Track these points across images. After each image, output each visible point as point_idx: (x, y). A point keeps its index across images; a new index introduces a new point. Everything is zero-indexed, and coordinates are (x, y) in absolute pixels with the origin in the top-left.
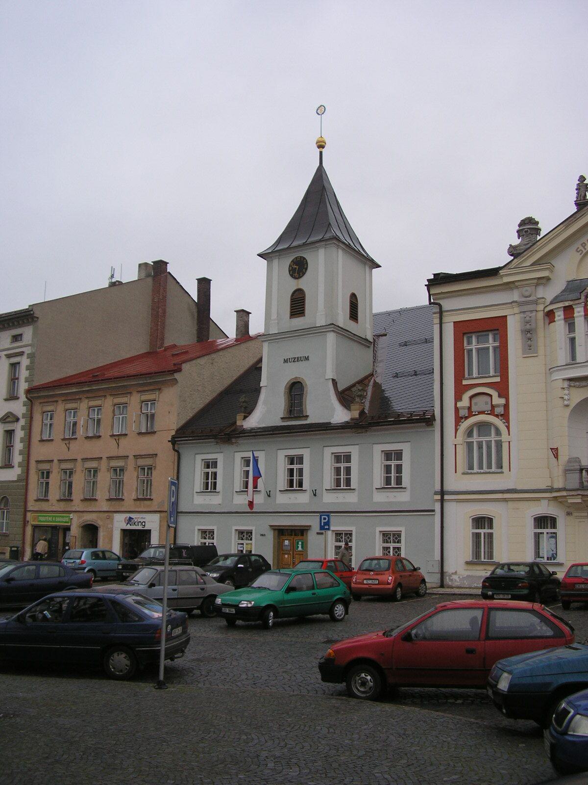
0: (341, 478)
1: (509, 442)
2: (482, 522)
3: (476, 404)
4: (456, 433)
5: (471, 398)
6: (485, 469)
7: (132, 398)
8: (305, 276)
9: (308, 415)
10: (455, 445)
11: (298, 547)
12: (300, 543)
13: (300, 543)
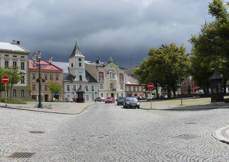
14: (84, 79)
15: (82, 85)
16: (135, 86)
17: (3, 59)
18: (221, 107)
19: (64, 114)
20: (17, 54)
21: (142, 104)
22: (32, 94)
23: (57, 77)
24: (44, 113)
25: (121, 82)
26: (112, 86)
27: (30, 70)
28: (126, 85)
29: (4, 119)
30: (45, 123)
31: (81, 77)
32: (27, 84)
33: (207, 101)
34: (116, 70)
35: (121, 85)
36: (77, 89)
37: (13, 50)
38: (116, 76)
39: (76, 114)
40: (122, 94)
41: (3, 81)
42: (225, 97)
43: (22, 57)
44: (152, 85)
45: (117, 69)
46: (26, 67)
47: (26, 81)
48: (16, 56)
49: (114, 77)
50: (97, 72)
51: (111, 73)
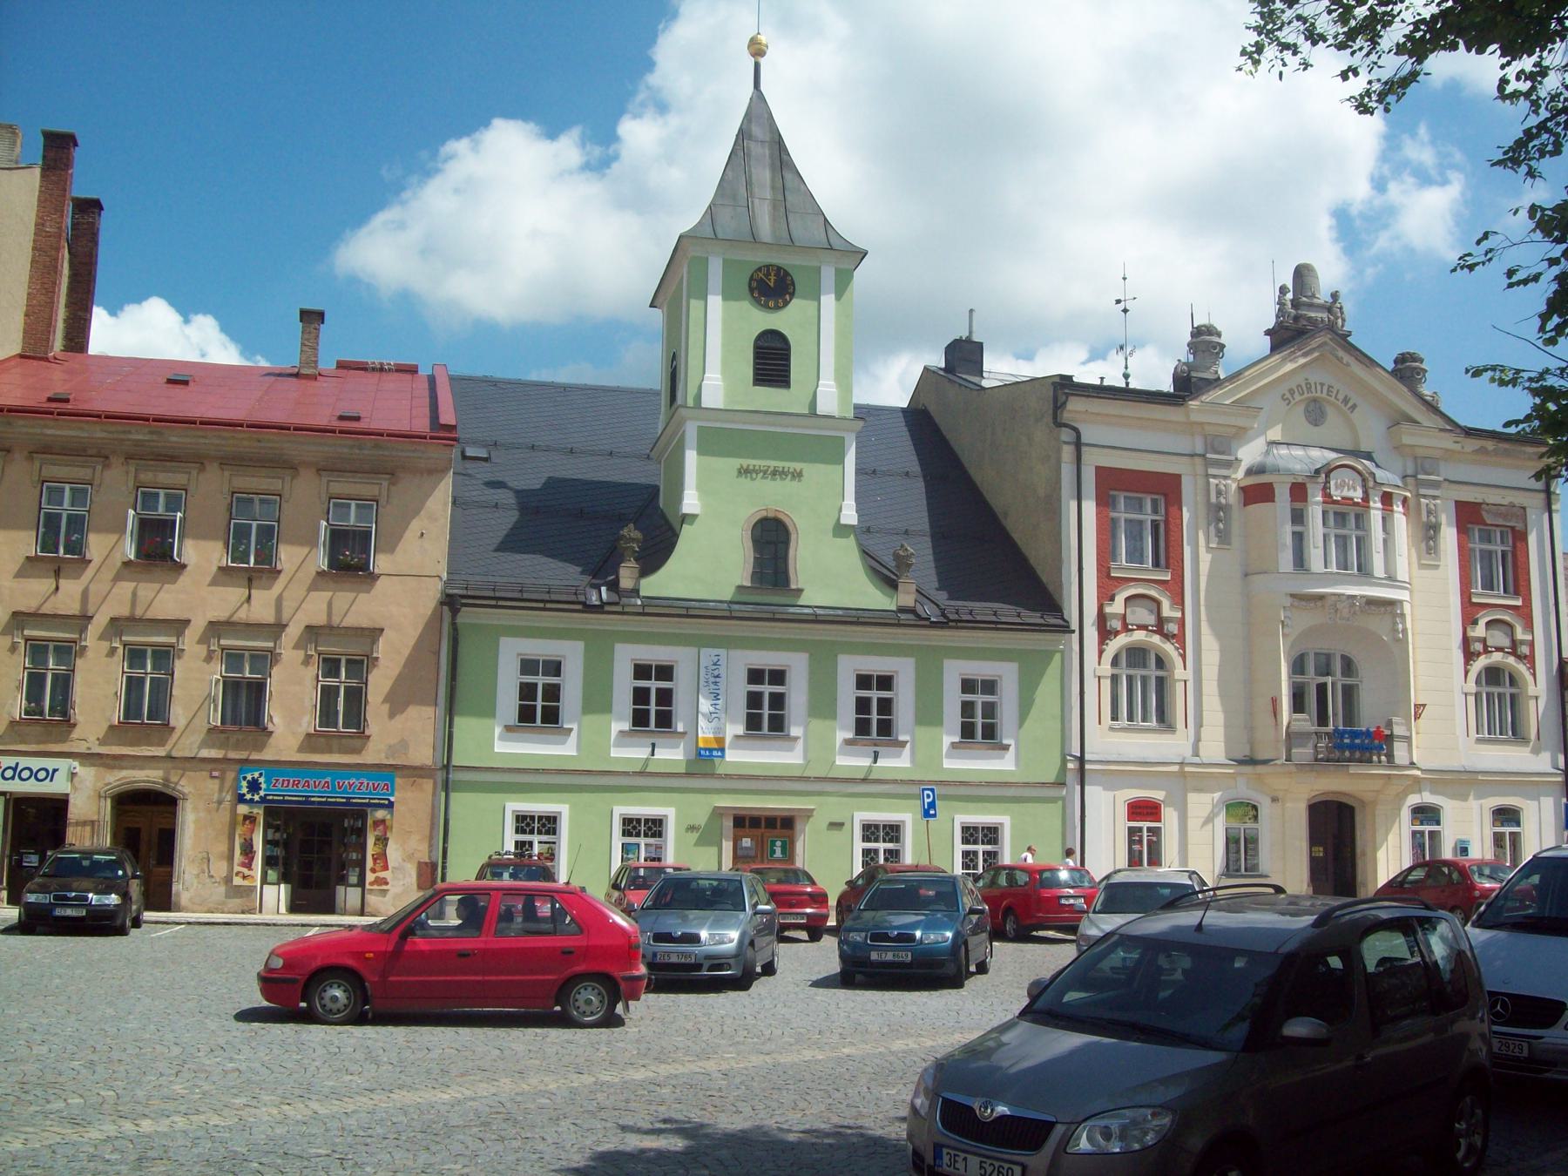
0: (535, 706)
1: (1185, 681)
2: (1143, 810)
3: (1133, 612)
4: (1100, 657)
5: (1127, 600)
6: (1123, 721)
7: (295, 481)
8: (747, 288)
9: (800, 587)
10: (1099, 677)
11: (774, 852)
12: (779, 843)
13: (779, 843)
18: (229, 702)
24: (1096, 1112)
25: (1479, 631)
35: (1136, 655)
40: (1506, 815)
45: (1408, 437)
50: (1067, 471)
51: (1299, 492)
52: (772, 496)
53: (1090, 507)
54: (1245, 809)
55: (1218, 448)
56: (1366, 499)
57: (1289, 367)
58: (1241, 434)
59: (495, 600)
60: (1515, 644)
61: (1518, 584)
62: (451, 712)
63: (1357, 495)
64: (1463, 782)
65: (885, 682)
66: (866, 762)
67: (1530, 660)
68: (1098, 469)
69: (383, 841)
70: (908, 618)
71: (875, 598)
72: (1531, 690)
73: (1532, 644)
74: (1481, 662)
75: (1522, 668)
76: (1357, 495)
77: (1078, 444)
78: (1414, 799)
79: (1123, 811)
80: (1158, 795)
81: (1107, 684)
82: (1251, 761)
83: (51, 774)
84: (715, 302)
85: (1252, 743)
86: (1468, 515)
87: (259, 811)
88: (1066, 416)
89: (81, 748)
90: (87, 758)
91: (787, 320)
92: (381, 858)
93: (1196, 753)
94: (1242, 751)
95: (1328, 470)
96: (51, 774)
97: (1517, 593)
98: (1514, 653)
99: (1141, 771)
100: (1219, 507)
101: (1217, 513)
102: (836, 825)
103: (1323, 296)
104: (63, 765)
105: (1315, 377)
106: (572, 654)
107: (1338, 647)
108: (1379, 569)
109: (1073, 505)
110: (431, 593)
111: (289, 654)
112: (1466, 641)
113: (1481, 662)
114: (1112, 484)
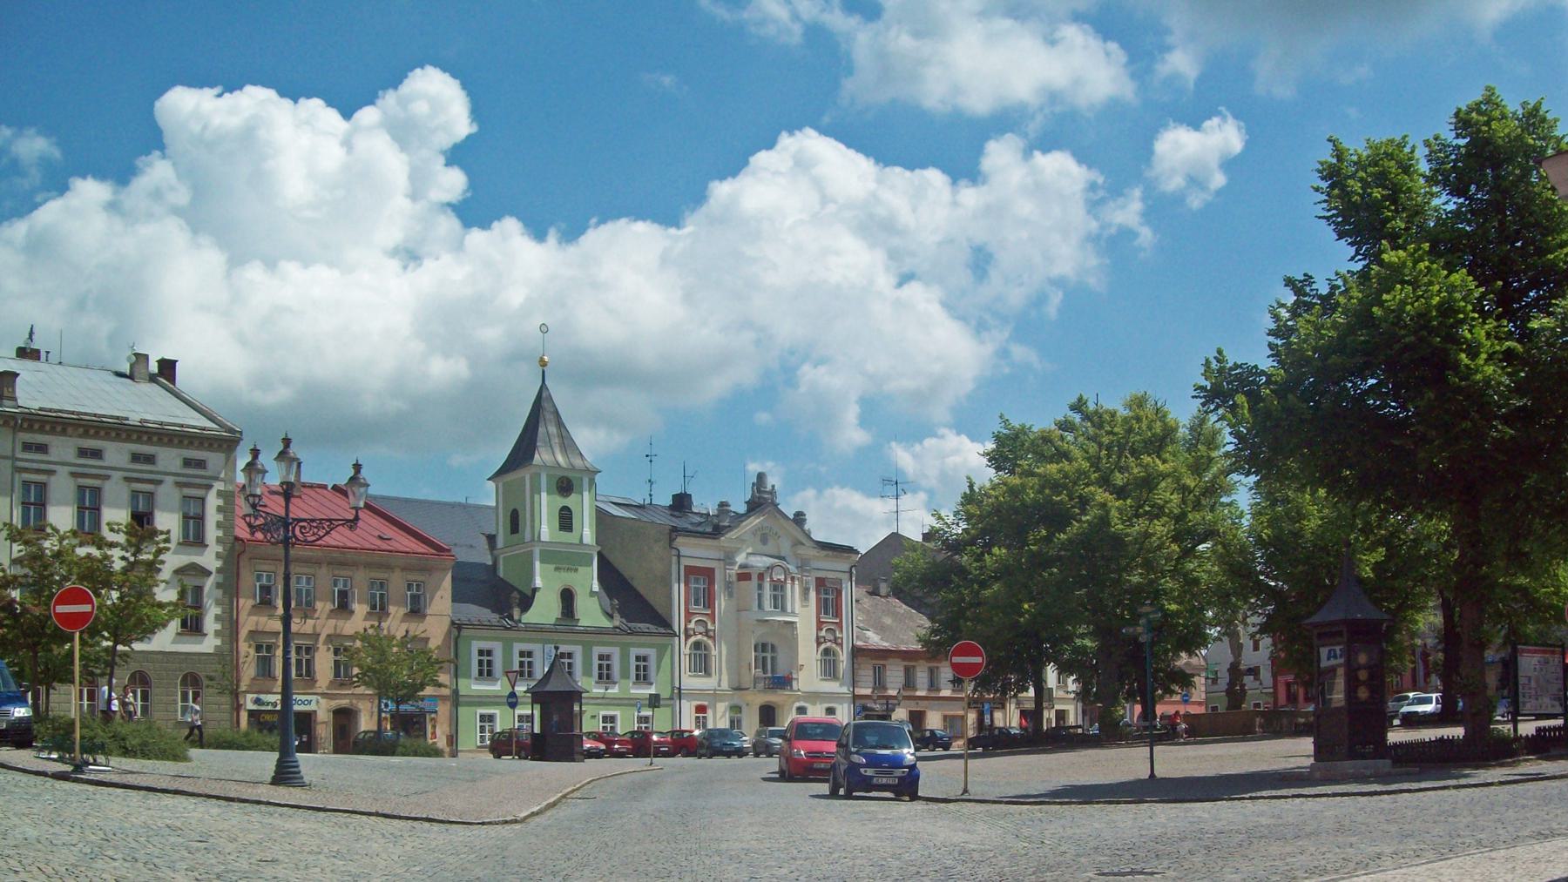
2: (701, 709)
14: (591, 612)
15: (578, 651)
16: (885, 658)
17: (63, 471)
19: (427, 825)
20: (53, 432)
21: (935, 775)
22: (251, 706)
23: (416, 599)
25: (823, 633)
26: (769, 655)
27: (238, 547)
28: (857, 652)
29: (60, 842)
30: (302, 865)
31: (567, 597)
32: (218, 642)
33: (1298, 751)
34: (796, 555)
36: (540, 670)
37: (134, 418)
38: (793, 592)
39: (506, 822)
41: (59, 615)
42: (1395, 736)
43: (187, 463)
44: (976, 653)
46: (212, 533)
47: (210, 624)
48: (150, 459)
49: (779, 603)
51: (761, 577)
52: (567, 579)
53: (682, 585)
54: (736, 709)
55: (728, 559)
56: (785, 579)
57: (758, 521)
58: (737, 551)
59: (472, 625)
60: (836, 639)
61: (838, 614)
62: (456, 676)
63: (782, 578)
64: (814, 697)
65: (489, 653)
66: (603, 691)
67: (841, 645)
68: (685, 566)
69: (434, 727)
70: (616, 631)
71: (605, 623)
72: (841, 658)
73: (842, 639)
74: (823, 647)
75: (838, 649)
76: (782, 578)
77: (679, 556)
78: (797, 704)
79: (694, 709)
80: (706, 703)
81: (687, 657)
82: (739, 689)
83: (310, 702)
84: (544, 495)
85: (739, 682)
86: (821, 583)
87: (388, 716)
88: (675, 544)
89: (319, 691)
90: (324, 695)
91: (571, 501)
92: (434, 733)
93: (719, 686)
94: (736, 686)
95: (770, 568)
96: (310, 702)
97: (837, 617)
98: (707, 635)
99: (700, 693)
100: (730, 582)
101: (728, 586)
102: (593, 717)
103: (769, 488)
104: (314, 698)
105: (765, 524)
106: (615, 652)
107: (770, 640)
108: (789, 610)
109: (677, 585)
110: (446, 623)
111: (322, 647)
112: (818, 638)
113: (823, 647)
114: (691, 571)
